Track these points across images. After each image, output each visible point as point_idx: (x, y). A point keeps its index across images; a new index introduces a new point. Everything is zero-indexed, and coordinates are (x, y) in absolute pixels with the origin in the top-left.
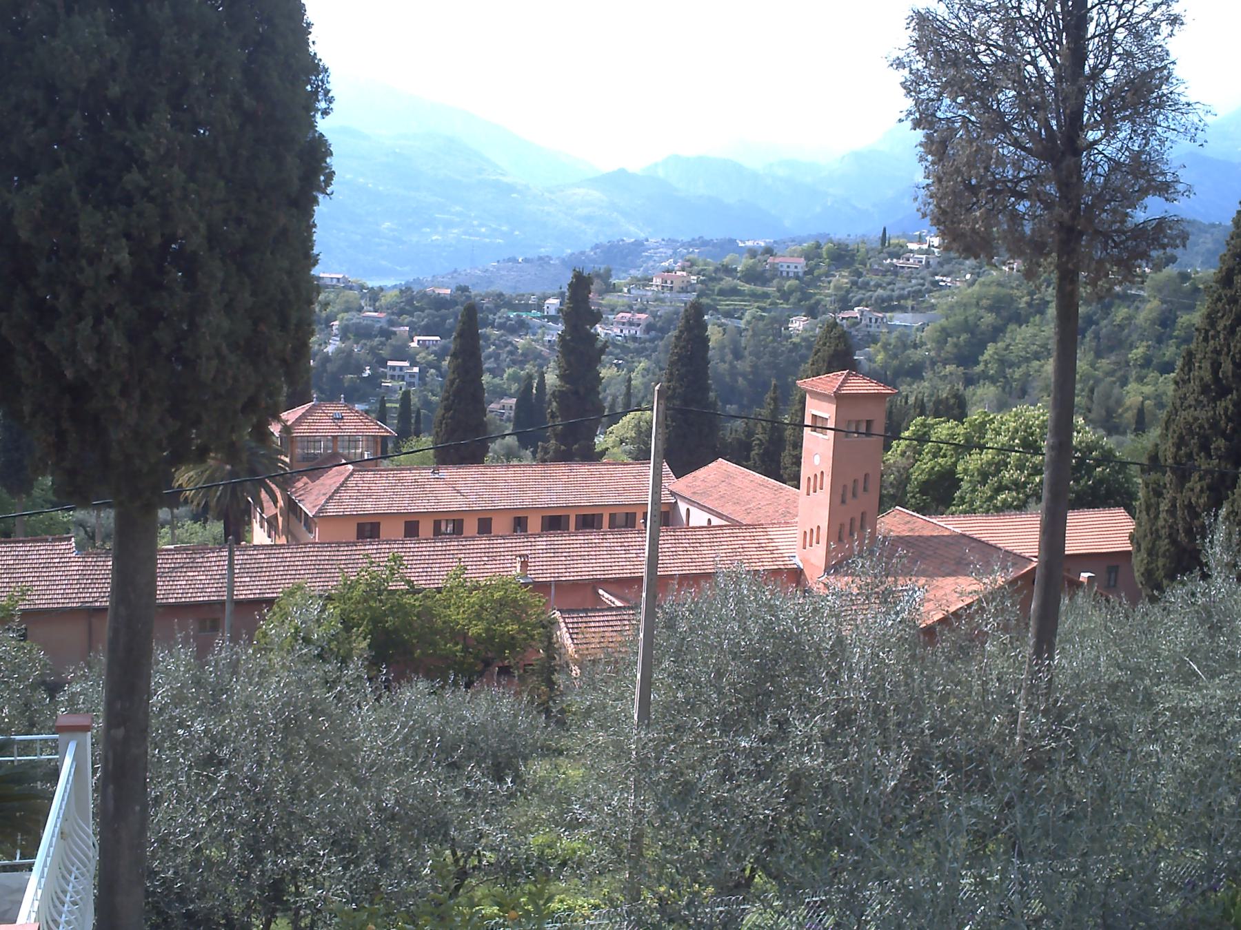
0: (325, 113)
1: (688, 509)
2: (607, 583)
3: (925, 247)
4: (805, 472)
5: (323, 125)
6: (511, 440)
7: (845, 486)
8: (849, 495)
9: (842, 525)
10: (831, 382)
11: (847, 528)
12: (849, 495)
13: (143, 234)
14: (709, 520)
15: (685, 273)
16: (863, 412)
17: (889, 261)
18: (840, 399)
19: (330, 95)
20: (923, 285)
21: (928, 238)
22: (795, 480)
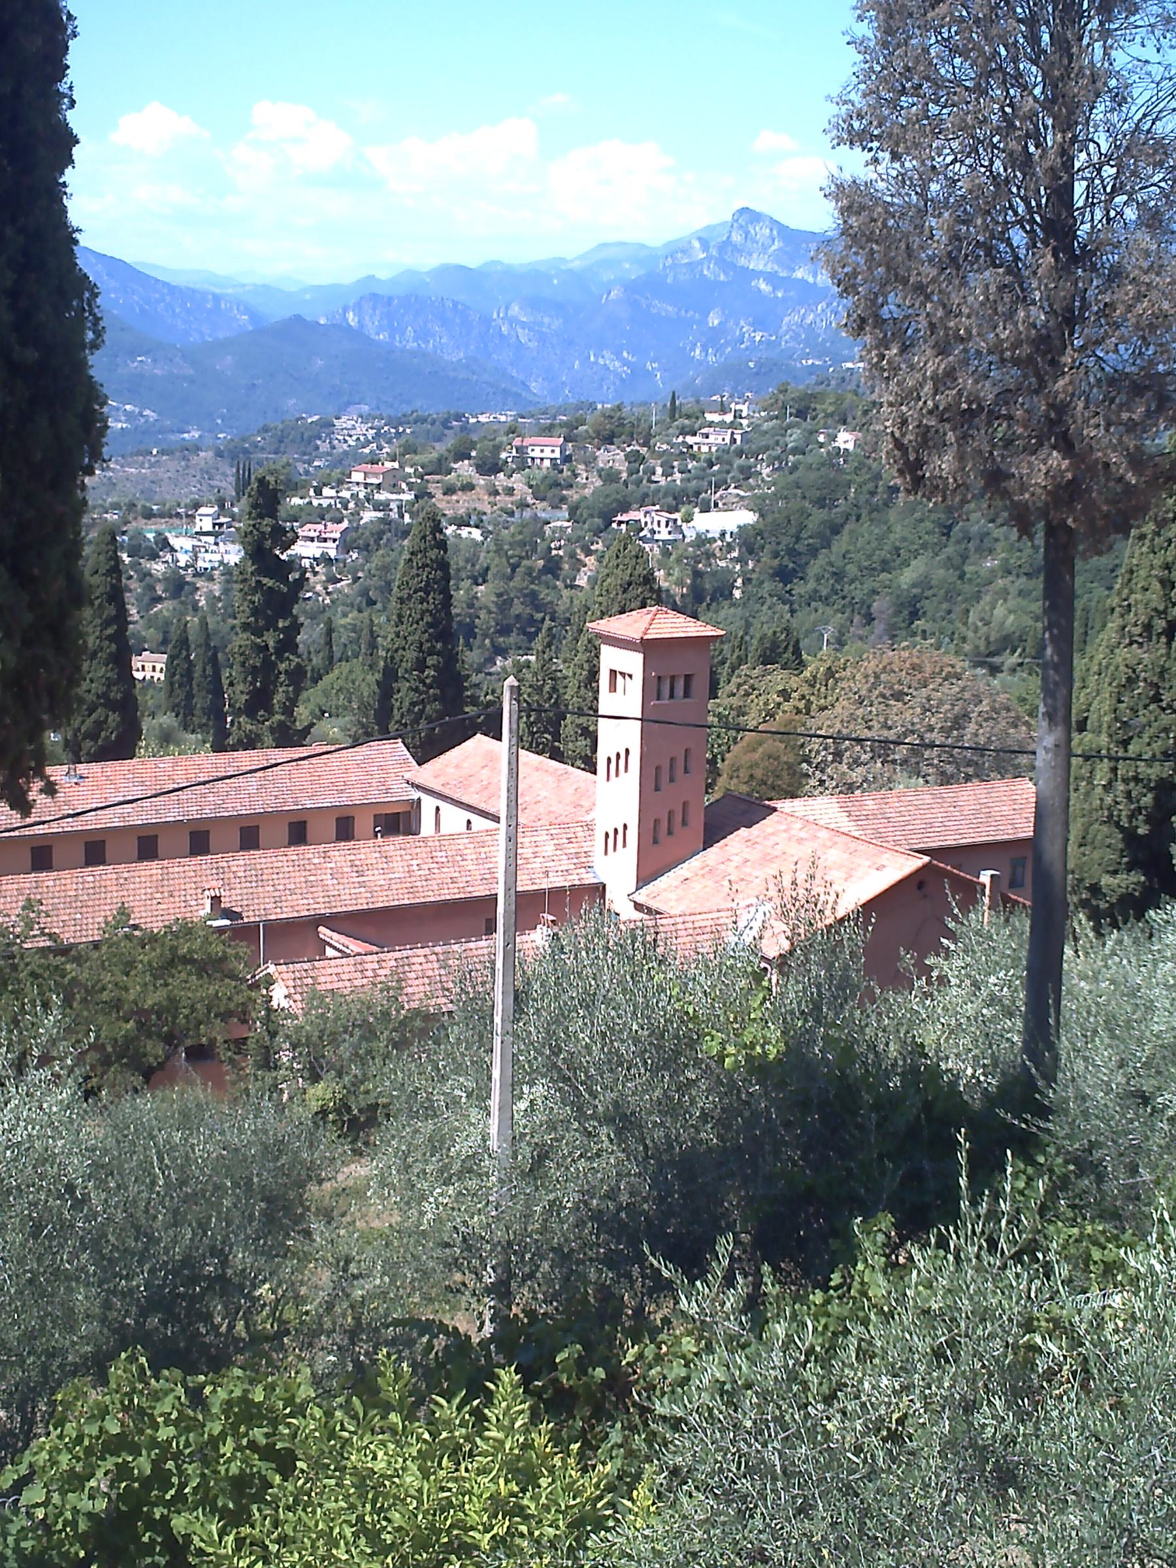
0: (95, 346)
1: (438, 809)
2: (336, 921)
3: (729, 418)
4: (604, 751)
5: (91, 372)
6: (167, 720)
7: (658, 769)
8: (665, 777)
9: (657, 822)
10: (632, 625)
11: (664, 825)
12: (665, 777)
13: (1041, 1159)
14: (469, 822)
15: (396, 465)
16: (681, 665)
17: (680, 439)
18: (649, 647)
19: (102, 324)
20: (728, 472)
21: (733, 406)
22: (590, 766)
